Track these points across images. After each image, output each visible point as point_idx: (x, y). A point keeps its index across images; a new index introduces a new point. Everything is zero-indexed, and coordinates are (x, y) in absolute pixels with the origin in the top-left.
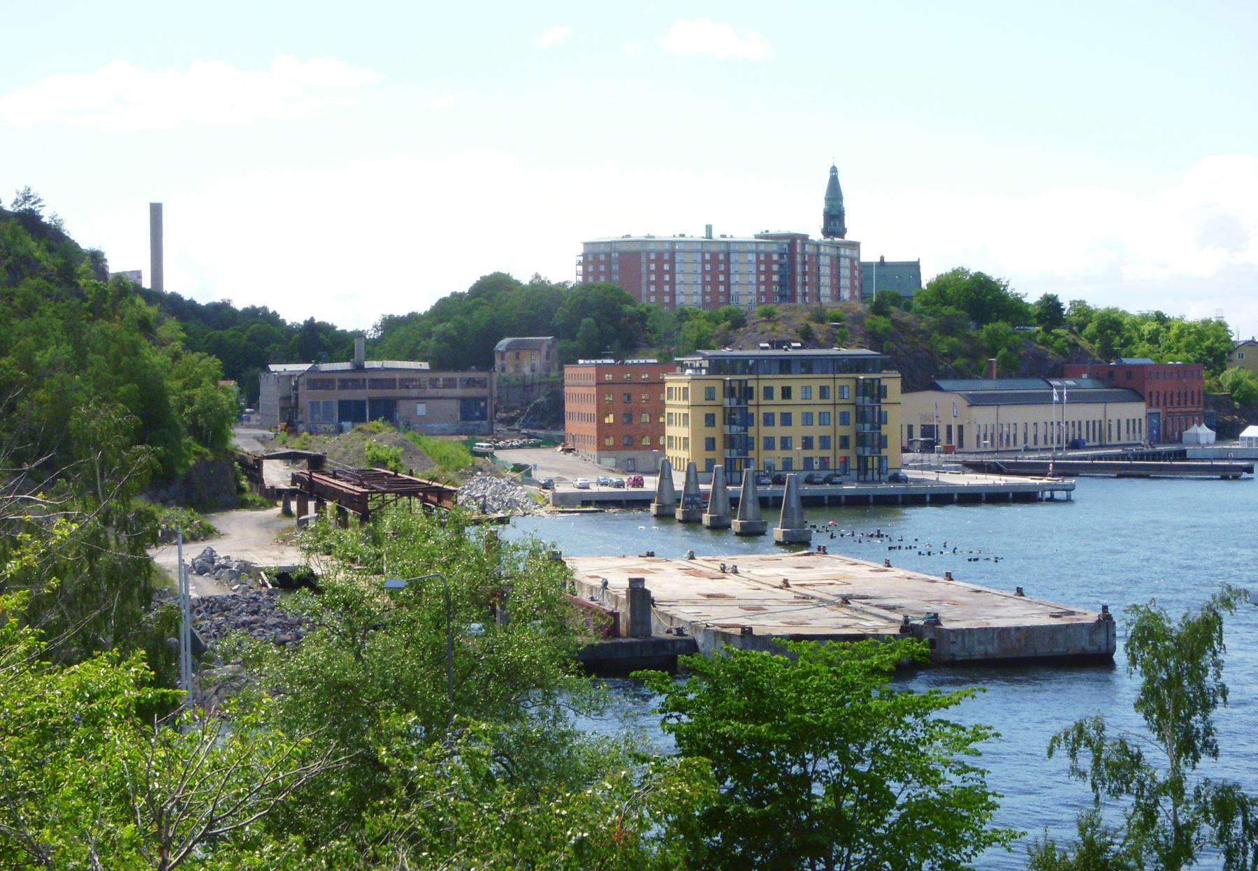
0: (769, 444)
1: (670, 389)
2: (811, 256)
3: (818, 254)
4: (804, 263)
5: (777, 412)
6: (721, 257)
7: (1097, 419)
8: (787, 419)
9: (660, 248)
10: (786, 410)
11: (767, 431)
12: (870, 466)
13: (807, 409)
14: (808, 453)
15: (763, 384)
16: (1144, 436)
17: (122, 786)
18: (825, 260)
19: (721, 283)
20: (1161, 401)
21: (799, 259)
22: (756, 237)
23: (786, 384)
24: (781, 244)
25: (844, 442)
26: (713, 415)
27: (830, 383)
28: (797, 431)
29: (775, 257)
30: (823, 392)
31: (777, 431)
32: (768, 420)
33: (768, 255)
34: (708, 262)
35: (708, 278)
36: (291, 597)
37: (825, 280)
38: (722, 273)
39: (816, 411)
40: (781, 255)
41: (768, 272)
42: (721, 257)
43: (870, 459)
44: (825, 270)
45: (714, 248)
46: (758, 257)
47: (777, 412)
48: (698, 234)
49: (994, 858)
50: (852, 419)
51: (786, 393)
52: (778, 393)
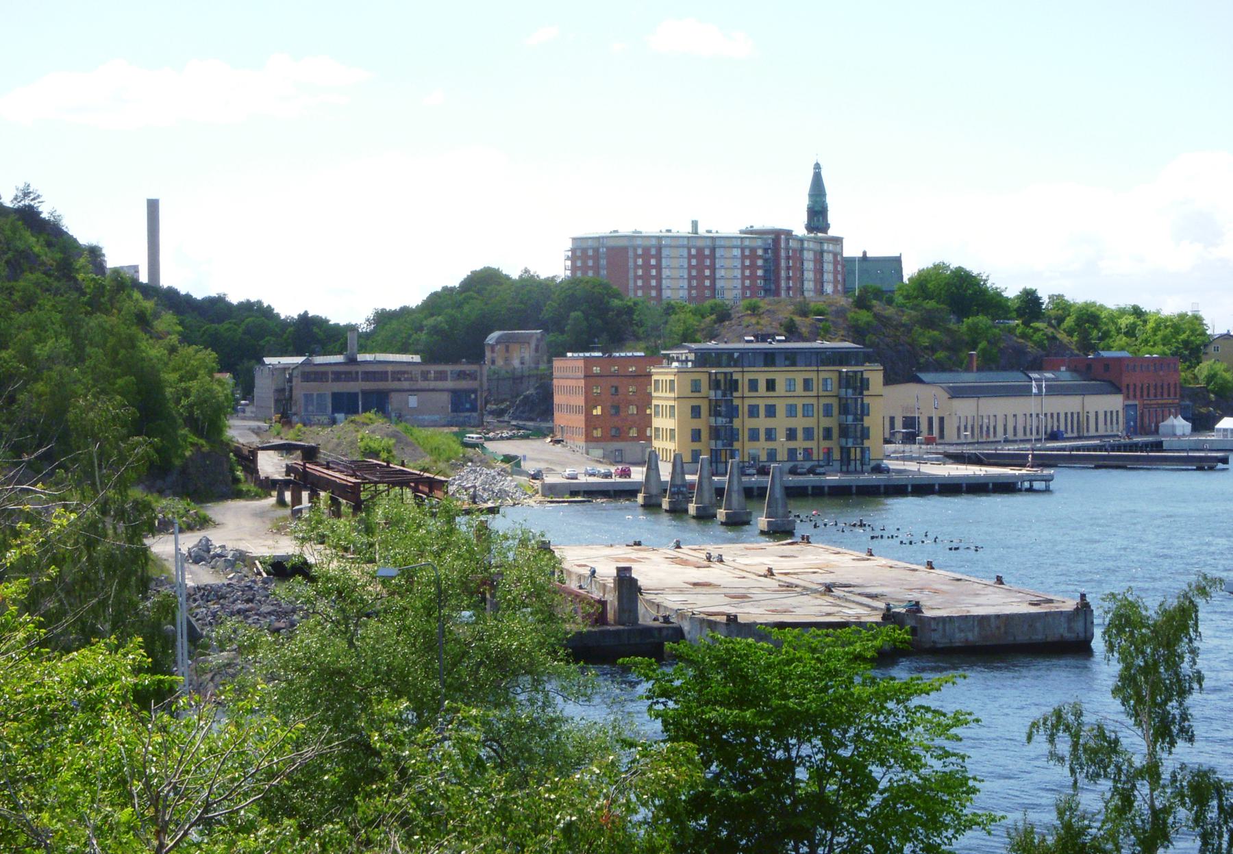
0: (754, 435)
1: (657, 381)
2: (794, 251)
3: (802, 249)
4: (788, 258)
5: (762, 404)
6: (707, 252)
7: (1075, 411)
8: (771, 411)
9: (647, 243)
10: (770, 402)
11: (751, 423)
12: (853, 457)
13: (791, 401)
14: (792, 444)
15: (748, 376)
16: (1121, 428)
17: (120, 771)
18: (808, 255)
19: (707, 277)
20: (1138, 394)
21: (783, 254)
22: (741, 232)
23: (771, 376)
24: (765, 240)
25: (828, 434)
26: (699, 407)
27: (813, 376)
28: (781, 423)
29: (760, 252)
30: (807, 384)
31: (762, 423)
32: (753, 412)
33: (753, 250)
34: (694, 257)
35: (694, 273)
36: (285, 585)
37: (809, 275)
38: (708, 267)
39: (799, 403)
40: (766, 250)
41: (753, 267)
42: (707, 252)
43: (853, 450)
44: (809, 265)
45: (700, 243)
46: (743, 252)
47: (762, 404)
48: (684, 229)
49: (974, 841)
50: (835, 411)
51: (771, 385)
52: (762, 386)
